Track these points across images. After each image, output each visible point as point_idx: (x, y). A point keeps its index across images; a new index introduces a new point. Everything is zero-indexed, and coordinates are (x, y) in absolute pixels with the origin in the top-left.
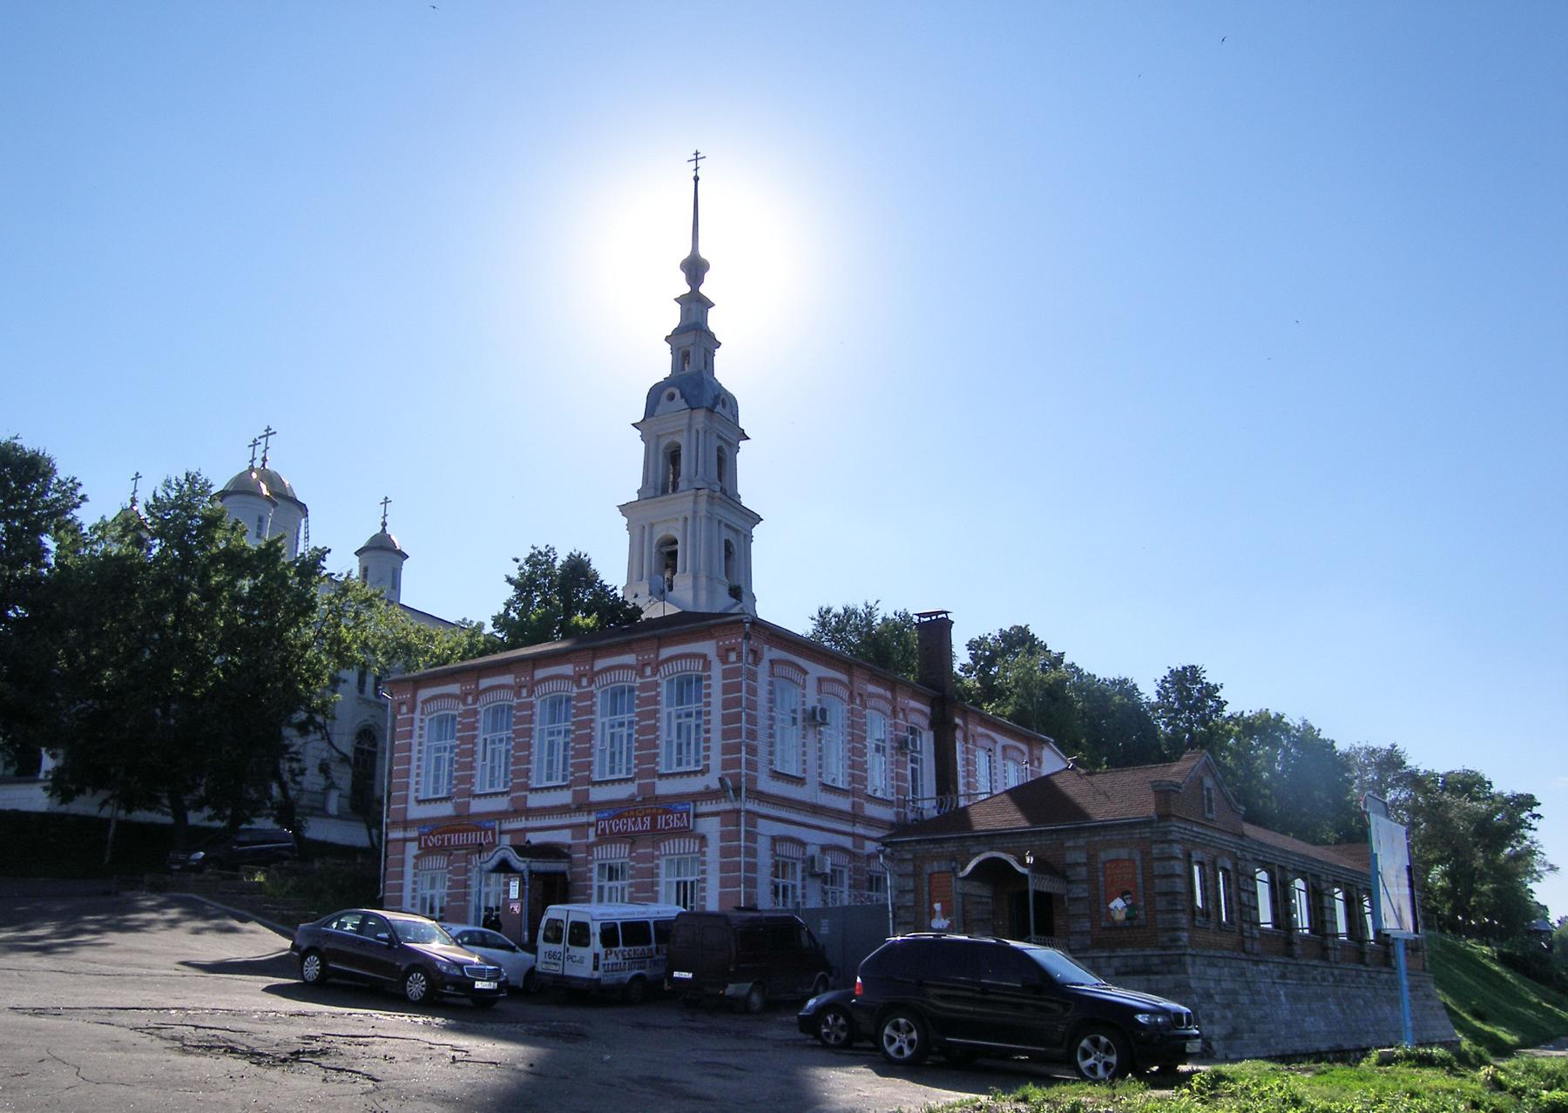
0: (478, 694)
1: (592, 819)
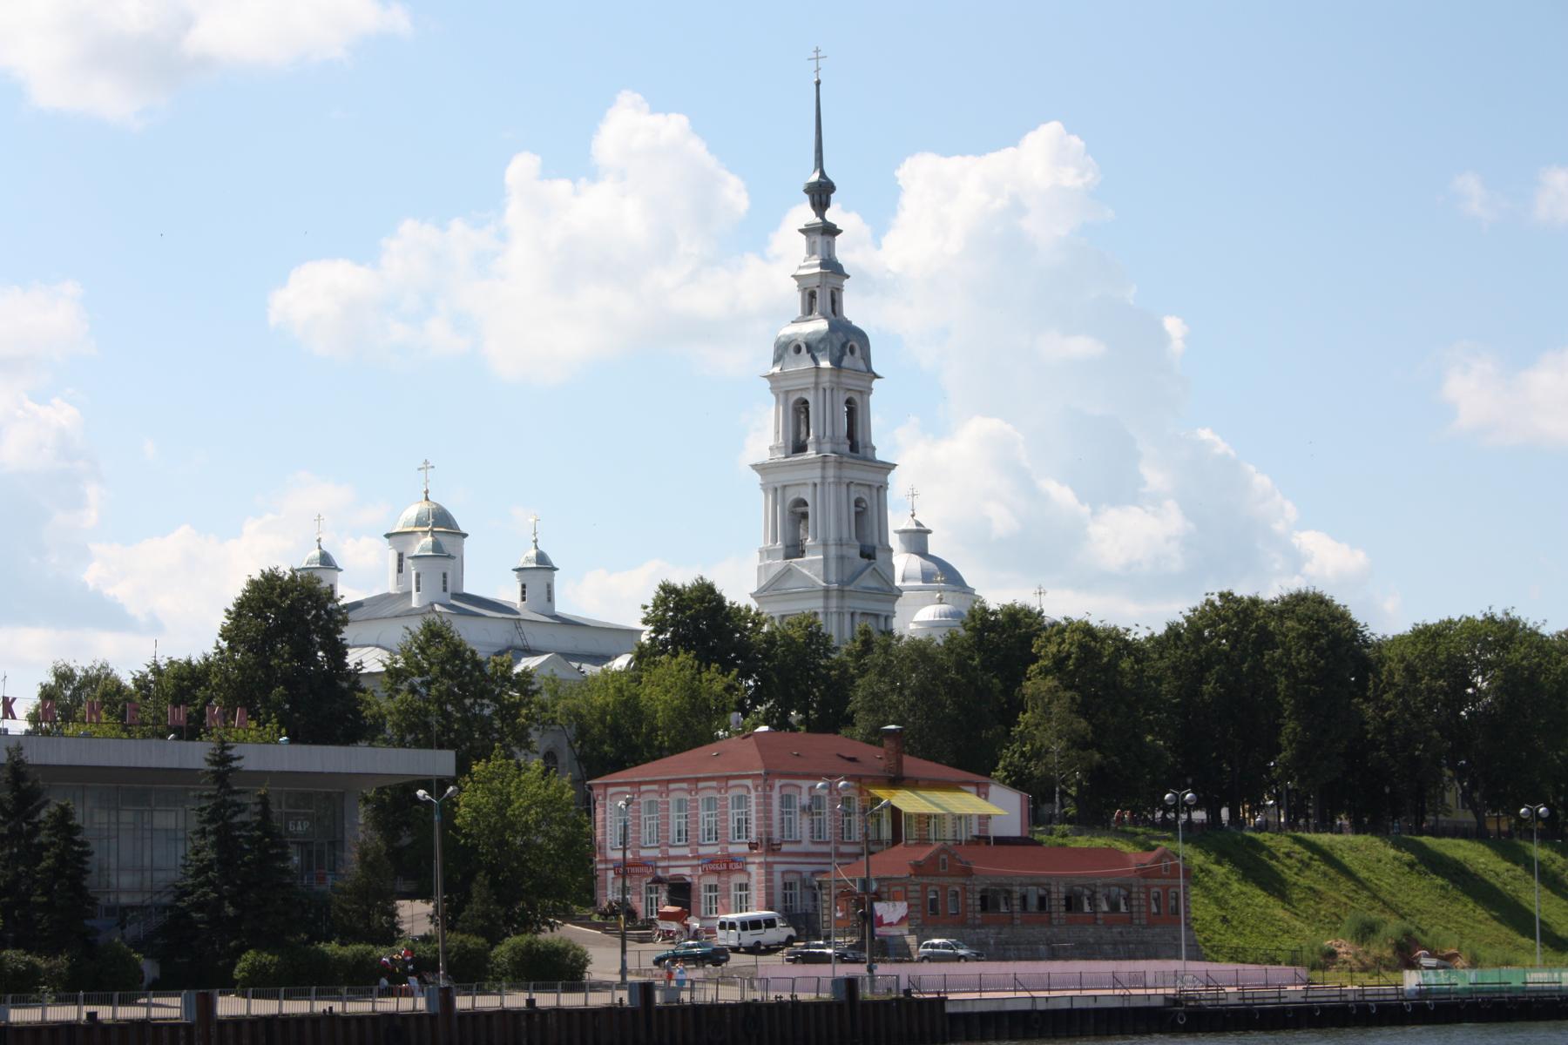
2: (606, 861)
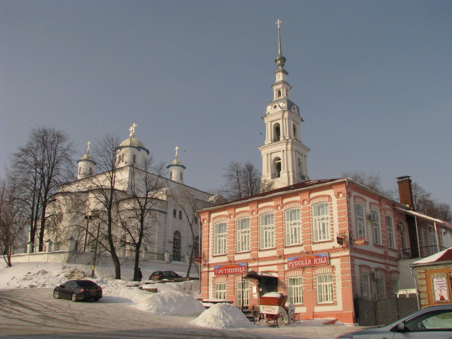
0: (235, 214)
1: (286, 261)
2: (209, 266)
